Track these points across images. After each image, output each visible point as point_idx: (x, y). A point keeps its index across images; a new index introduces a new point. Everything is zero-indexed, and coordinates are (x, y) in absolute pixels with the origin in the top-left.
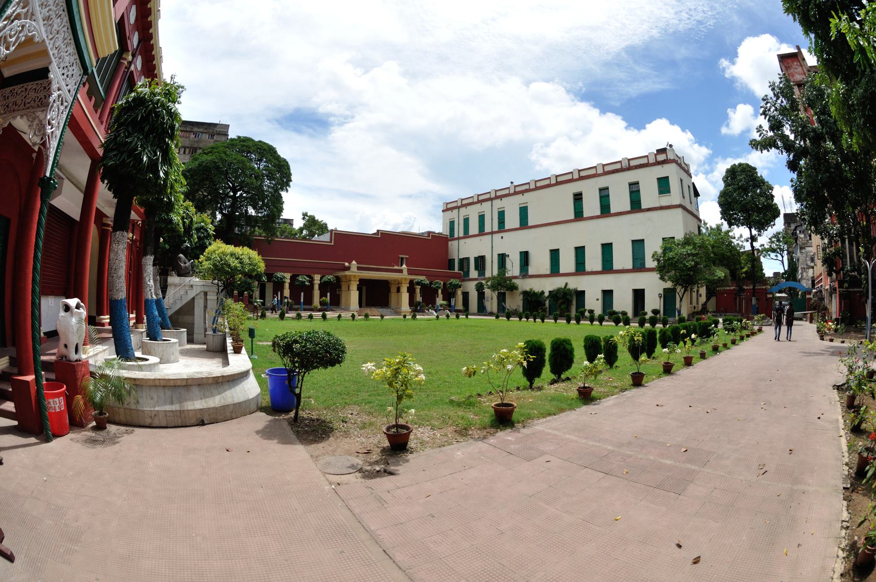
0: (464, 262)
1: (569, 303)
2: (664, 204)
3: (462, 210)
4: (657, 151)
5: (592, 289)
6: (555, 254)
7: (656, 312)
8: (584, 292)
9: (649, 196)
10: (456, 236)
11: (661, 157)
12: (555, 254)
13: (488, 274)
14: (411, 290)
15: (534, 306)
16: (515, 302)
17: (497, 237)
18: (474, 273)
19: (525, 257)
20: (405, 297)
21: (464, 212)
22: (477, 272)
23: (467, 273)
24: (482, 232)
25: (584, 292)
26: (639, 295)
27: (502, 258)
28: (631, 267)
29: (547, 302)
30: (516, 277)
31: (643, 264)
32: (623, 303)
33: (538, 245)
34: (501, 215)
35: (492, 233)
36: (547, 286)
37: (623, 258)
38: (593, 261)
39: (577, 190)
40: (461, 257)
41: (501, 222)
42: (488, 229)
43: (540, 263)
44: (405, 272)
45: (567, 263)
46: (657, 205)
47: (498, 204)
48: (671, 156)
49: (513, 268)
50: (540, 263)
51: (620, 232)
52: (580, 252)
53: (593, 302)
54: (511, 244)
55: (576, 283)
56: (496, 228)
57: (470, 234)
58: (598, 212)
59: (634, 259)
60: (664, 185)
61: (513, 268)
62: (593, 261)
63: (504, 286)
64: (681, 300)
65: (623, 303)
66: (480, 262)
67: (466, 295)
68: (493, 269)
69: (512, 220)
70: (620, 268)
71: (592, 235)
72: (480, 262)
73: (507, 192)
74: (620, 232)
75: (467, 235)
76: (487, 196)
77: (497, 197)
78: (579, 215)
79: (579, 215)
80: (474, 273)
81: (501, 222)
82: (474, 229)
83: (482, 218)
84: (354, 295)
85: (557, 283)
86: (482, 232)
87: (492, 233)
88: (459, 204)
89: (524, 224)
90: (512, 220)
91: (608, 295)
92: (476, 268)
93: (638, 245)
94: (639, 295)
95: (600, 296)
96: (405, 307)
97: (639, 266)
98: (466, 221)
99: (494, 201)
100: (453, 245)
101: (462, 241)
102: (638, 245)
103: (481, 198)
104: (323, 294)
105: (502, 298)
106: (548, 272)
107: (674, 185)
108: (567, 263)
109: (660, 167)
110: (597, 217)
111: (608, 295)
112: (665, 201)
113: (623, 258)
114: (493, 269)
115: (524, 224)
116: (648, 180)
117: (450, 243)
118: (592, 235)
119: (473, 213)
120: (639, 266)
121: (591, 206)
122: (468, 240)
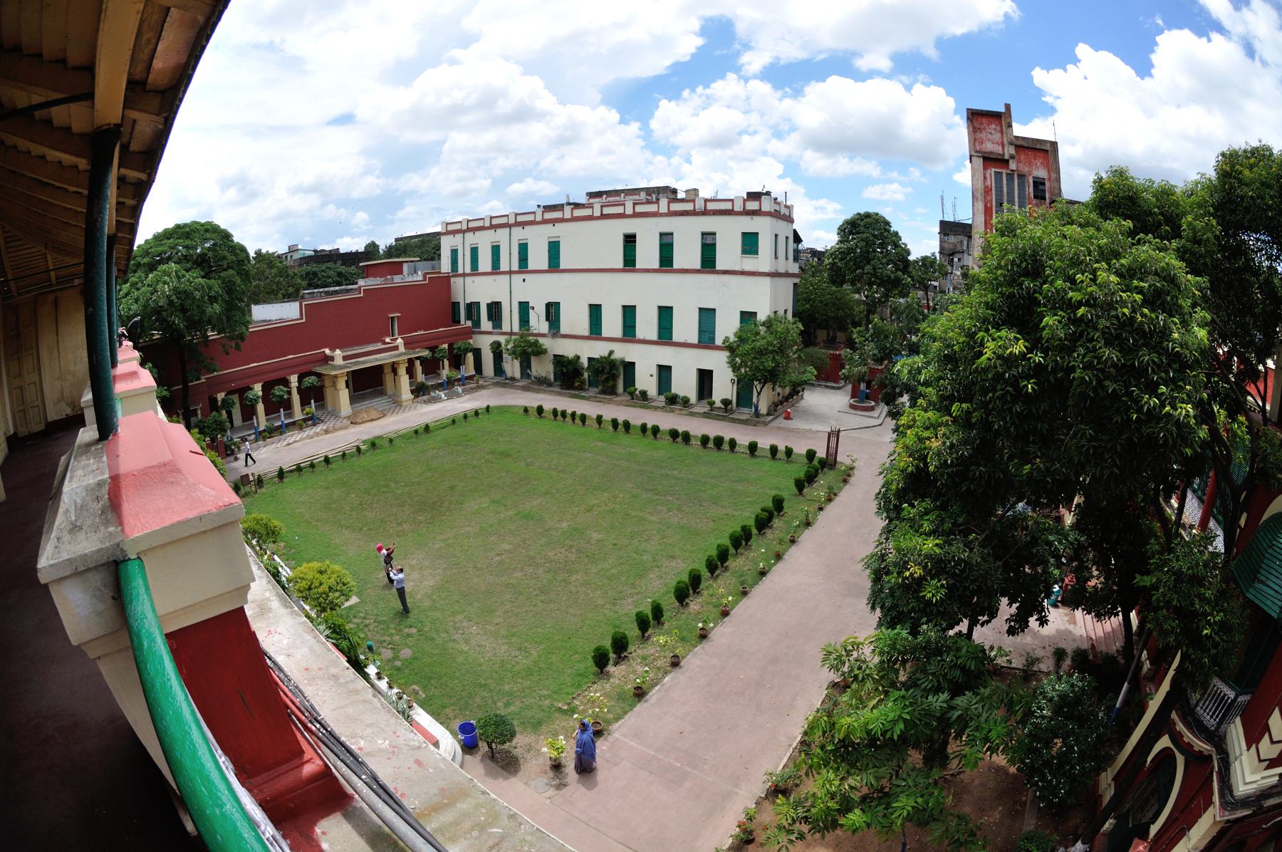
0: (473, 308)
1: (614, 377)
2: (747, 268)
3: (469, 235)
4: (749, 194)
5: (646, 361)
6: (595, 311)
7: (726, 402)
8: (633, 364)
9: (729, 254)
10: (460, 271)
11: (752, 205)
12: (595, 311)
13: (506, 328)
14: (410, 371)
15: (568, 375)
16: (544, 368)
17: (517, 279)
18: (486, 325)
19: (552, 311)
20: (404, 380)
21: (471, 238)
22: (490, 323)
23: (477, 323)
24: (496, 269)
25: (633, 364)
26: (705, 378)
27: (524, 308)
28: (696, 341)
29: (586, 375)
30: (543, 335)
31: (713, 339)
32: (685, 384)
33: (574, 300)
34: (523, 248)
35: (510, 273)
36: (588, 351)
37: (686, 327)
38: (647, 326)
39: (630, 231)
40: (468, 301)
41: (523, 259)
42: (504, 266)
43: (574, 319)
44: (402, 349)
45: (612, 324)
46: (737, 268)
47: (518, 233)
48: (767, 205)
49: (538, 323)
50: (574, 319)
51: (687, 295)
52: (629, 313)
53: (646, 380)
54: (538, 290)
55: (624, 352)
56: (515, 267)
57: (481, 270)
58: (694, 339)
59: (701, 332)
60: (750, 243)
61: (538, 323)
62: (647, 326)
63: (528, 351)
64: (759, 394)
65: (685, 384)
66: (495, 310)
67: (477, 353)
68: (511, 321)
69: (538, 258)
70: (682, 340)
71: (646, 292)
72: (495, 310)
73: (531, 218)
74: (687, 295)
75: (475, 271)
76: (504, 220)
77: (517, 224)
78: (629, 262)
79: (629, 262)
80: (486, 325)
81: (523, 259)
82: (485, 264)
83: (496, 250)
84: (344, 394)
85: (598, 350)
86: (496, 269)
87: (510, 273)
88: (465, 227)
89: (554, 264)
90: (538, 258)
91: (664, 372)
92: (490, 318)
93: (707, 315)
94: (705, 378)
95: (655, 371)
96: (406, 393)
97: (706, 339)
98: (474, 251)
99: (513, 229)
100: (457, 283)
101: (468, 279)
102: (707, 315)
103: (495, 222)
104: (304, 403)
105: (525, 366)
106: (586, 333)
107: (765, 244)
108: (612, 324)
109: (748, 218)
110: (655, 271)
111: (664, 372)
112: (749, 264)
113: (686, 327)
114: (511, 321)
115: (554, 264)
116: (729, 234)
117: (453, 280)
118: (646, 292)
119: (484, 241)
120: (706, 339)
121: (648, 254)
122: (477, 279)
